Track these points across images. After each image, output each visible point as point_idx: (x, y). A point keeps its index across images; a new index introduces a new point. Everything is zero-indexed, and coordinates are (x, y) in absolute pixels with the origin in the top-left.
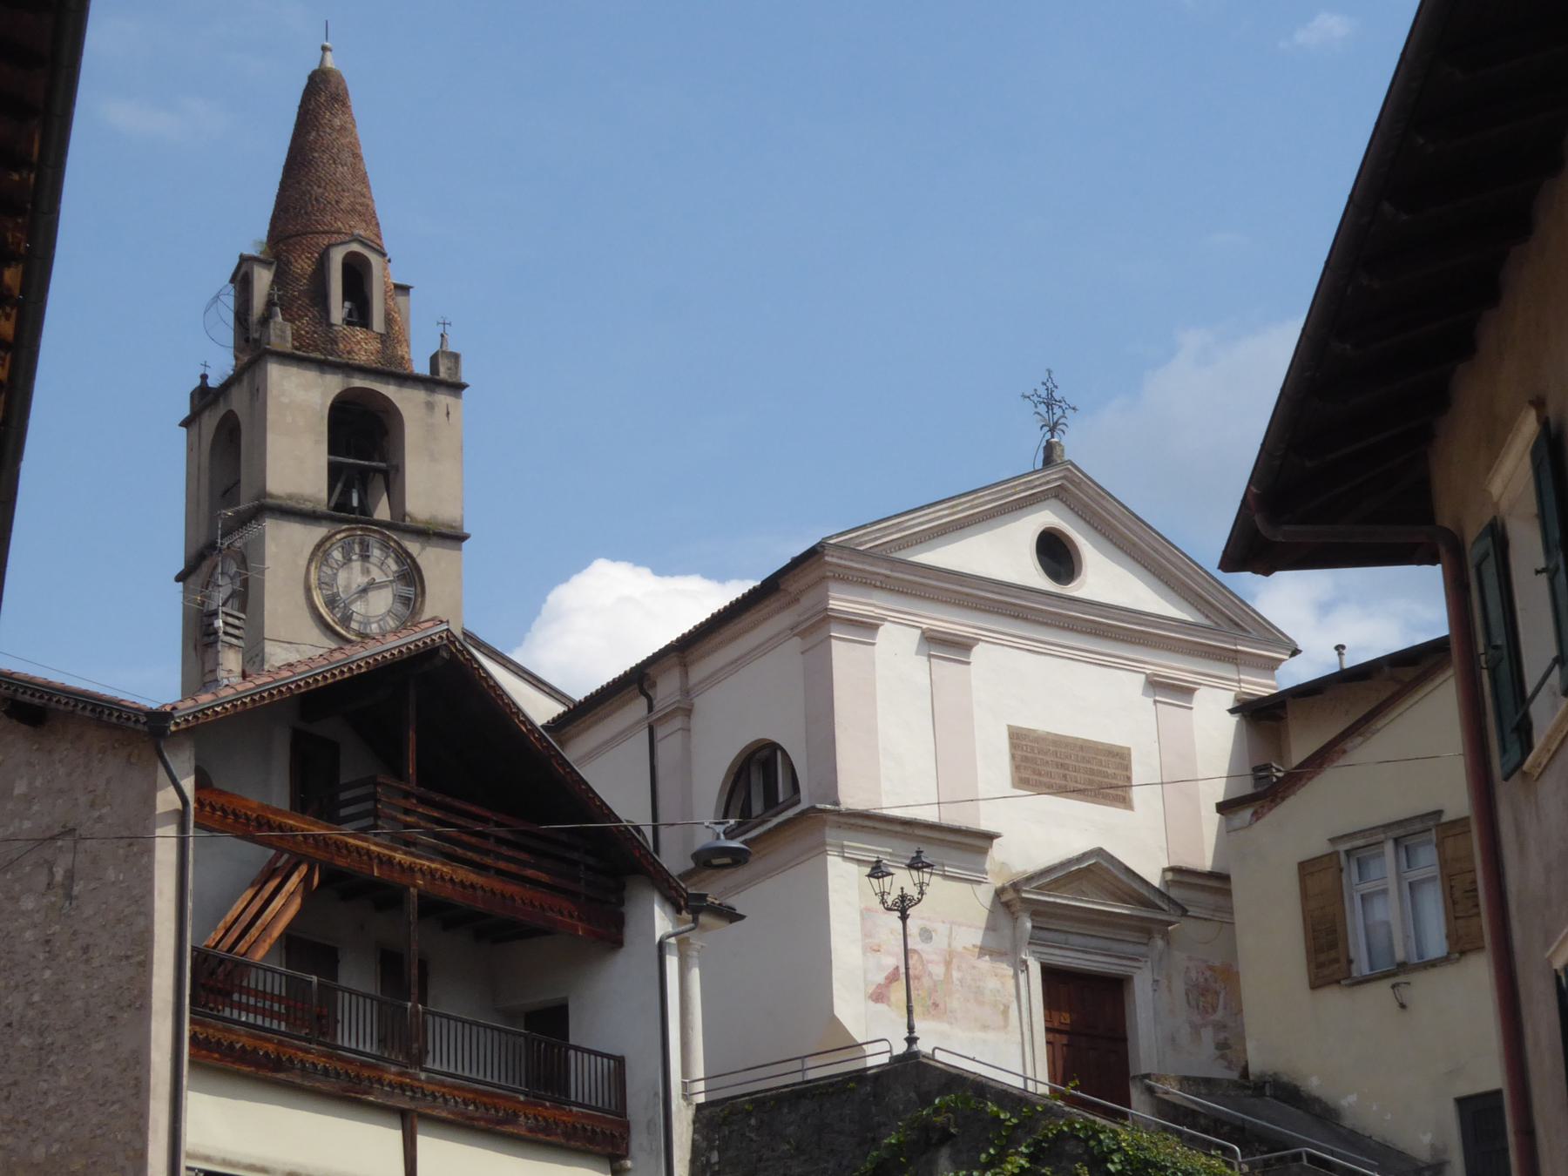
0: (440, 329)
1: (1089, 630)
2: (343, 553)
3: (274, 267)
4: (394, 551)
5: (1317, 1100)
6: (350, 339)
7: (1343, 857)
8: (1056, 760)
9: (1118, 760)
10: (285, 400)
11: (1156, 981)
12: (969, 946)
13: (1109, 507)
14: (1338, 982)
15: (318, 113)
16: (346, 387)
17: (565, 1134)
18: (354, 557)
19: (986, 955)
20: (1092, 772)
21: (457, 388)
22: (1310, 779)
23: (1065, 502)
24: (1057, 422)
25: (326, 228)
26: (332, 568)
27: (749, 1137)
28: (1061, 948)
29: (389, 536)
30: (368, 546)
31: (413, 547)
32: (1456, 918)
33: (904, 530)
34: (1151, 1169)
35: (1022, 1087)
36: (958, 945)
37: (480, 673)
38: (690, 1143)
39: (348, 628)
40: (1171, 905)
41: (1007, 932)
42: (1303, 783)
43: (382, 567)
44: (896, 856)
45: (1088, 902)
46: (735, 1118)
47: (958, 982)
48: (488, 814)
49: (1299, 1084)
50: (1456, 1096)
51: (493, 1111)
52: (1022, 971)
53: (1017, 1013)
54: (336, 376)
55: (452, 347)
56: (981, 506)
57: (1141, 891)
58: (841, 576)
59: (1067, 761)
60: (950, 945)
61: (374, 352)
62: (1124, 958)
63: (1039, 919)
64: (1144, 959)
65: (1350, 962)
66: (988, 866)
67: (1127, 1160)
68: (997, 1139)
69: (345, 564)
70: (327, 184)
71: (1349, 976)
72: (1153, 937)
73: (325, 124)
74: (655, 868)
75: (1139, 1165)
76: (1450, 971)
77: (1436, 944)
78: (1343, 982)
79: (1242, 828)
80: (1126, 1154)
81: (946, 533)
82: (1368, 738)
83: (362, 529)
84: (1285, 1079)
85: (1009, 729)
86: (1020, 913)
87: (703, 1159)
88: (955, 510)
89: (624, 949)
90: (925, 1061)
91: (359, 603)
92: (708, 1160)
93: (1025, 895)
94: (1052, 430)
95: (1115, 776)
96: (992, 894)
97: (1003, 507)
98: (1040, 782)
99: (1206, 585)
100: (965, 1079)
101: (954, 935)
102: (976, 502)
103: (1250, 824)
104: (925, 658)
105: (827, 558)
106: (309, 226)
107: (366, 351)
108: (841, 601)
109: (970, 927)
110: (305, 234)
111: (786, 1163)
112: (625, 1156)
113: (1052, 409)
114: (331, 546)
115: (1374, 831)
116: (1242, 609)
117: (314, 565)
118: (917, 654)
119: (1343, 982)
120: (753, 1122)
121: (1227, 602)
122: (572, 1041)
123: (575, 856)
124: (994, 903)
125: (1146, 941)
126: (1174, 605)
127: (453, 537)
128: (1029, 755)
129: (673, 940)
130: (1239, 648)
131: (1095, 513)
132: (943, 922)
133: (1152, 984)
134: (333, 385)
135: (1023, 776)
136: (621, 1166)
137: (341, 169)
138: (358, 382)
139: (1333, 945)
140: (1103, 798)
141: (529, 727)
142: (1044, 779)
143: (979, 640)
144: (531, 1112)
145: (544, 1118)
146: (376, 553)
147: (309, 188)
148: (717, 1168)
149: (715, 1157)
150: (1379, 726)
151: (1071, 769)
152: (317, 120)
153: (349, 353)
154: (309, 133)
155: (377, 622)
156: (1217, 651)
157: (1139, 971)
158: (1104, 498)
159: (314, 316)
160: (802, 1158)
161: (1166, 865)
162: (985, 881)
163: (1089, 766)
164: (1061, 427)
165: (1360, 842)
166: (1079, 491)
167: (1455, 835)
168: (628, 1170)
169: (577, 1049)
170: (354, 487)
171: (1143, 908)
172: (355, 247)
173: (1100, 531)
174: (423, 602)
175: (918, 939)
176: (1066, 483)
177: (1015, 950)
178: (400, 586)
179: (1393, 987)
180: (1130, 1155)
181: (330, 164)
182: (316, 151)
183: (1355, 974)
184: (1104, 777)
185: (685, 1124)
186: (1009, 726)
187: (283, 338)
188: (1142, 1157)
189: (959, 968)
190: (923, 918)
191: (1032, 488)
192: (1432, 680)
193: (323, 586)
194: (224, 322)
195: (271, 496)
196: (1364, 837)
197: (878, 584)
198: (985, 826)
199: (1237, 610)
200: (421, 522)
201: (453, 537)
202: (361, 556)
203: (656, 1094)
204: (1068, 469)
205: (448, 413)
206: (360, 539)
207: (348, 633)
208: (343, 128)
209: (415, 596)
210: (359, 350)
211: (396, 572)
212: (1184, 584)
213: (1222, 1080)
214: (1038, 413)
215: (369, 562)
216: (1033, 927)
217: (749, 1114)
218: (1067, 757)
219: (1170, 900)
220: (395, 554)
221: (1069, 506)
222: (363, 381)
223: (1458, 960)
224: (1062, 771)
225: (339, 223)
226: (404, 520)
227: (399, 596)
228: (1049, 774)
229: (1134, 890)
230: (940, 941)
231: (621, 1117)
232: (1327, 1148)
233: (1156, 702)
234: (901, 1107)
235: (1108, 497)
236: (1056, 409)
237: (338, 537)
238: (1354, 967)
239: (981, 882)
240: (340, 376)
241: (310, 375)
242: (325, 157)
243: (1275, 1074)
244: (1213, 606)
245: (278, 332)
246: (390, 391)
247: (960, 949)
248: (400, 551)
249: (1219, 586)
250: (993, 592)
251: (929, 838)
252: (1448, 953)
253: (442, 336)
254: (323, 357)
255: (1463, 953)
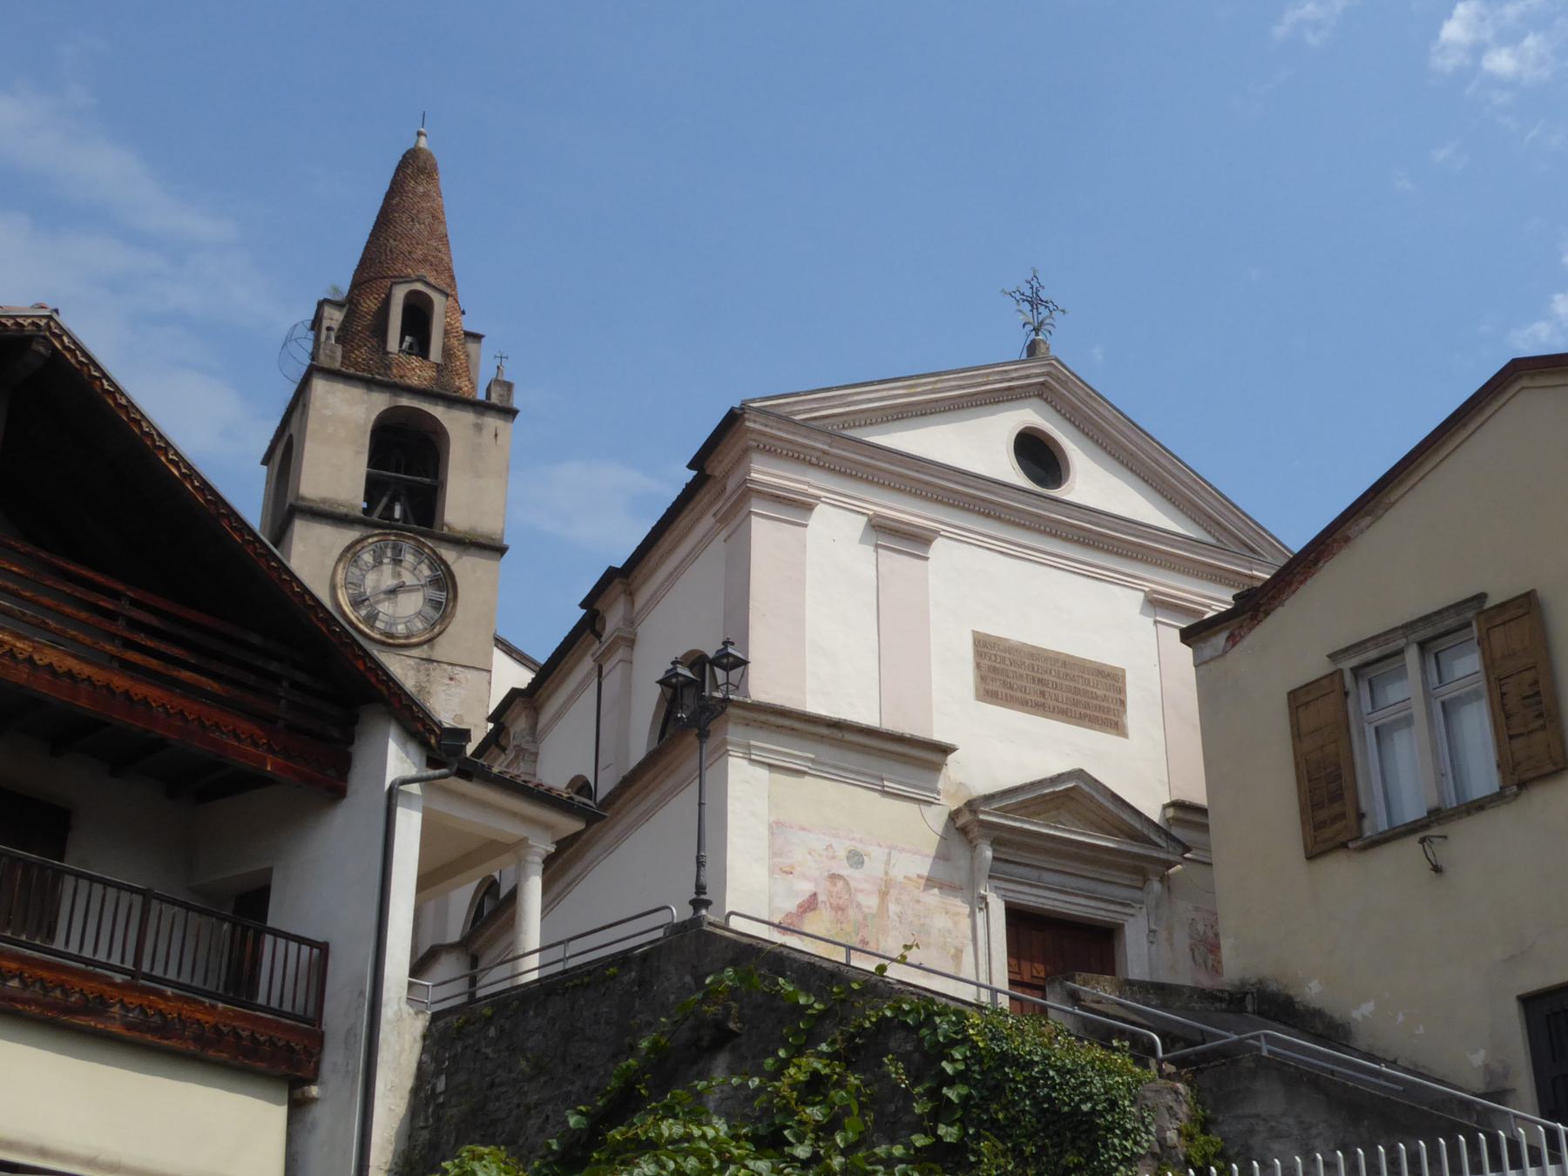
0: (498, 362)
1: (1076, 538)
2: (374, 557)
3: (345, 310)
4: (428, 557)
5: (1318, 1014)
6: (405, 366)
7: (1348, 678)
8: (1032, 674)
9: (1109, 682)
10: (328, 413)
11: (1152, 931)
12: (913, 875)
13: (1101, 409)
14: (1344, 846)
15: (404, 182)
16: (392, 406)
17: (199, 1039)
18: (386, 561)
19: (935, 887)
20: (1077, 691)
21: (509, 413)
22: (1302, 582)
23: (1049, 403)
24: (1042, 322)
25: (395, 273)
26: (361, 569)
27: (485, 1053)
28: (1031, 885)
29: (423, 543)
30: (401, 551)
31: (449, 555)
32: (1511, 737)
33: (848, 404)
34: (1010, 1068)
35: (844, 961)
36: (898, 873)
37: (102, 384)
38: (414, 1065)
39: (372, 627)
40: (1169, 842)
41: (964, 863)
42: (1293, 588)
43: (414, 570)
44: (823, 764)
45: (1064, 830)
46: (471, 1028)
47: (896, 918)
48: (120, 587)
49: (1292, 993)
50: (1520, 993)
51: (58, 993)
52: (981, 909)
53: (972, 958)
54: (383, 395)
55: (506, 378)
56: (947, 391)
57: (1132, 822)
58: (767, 447)
59: (1046, 677)
60: (886, 873)
61: (428, 378)
62: (1113, 902)
63: (1003, 849)
64: (1138, 906)
65: (1361, 816)
66: (940, 785)
67: (977, 1056)
68: (793, 1035)
69: (374, 566)
70: (403, 238)
71: (1359, 836)
72: (1149, 880)
73: (409, 191)
74: (389, 688)
75: (992, 1063)
76: (1501, 817)
77: (1483, 777)
78: (1351, 845)
79: (1213, 659)
80: (974, 1046)
81: (903, 418)
82: (1380, 517)
83: (396, 535)
84: (1274, 987)
85: (974, 635)
86: (980, 841)
87: (428, 1087)
88: (913, 390)
89: (345, 801)
90: (710, 929)
91: (387, 604)
92: (433, 1089)
93: (982, 817)
94: (1037, 330)
95: (1105, 698)
96: (945, 817)
97: (976, 397)
98: (1012, 697)
99: (1216, 503)
100: (760, 950)
101: (893, 861)
102: (939, 385)
103: (1225, 652)
104: (872, 548)
105: (747, 424)
106: (379, 272)
107: (419, 377)
108: (764, 472)
109: (915, 854)
110: (375, 279)
111: (521, 1088)
112: (313, 1080)
113: (1037, 309)
114: (363, 548)
115: (1389, 636)
116: (1259, 534)
117: (341, 565)
118: (862, 541)
119: (1351, 845)
120: (492, 1032)
121: (1240, 524)
122: (270, 923)
123: (274, 667)
124: (947, 826)
125: (1140, 885)
126: (1173, 520)
127: (494, 549)
128: (998, 665)
129: (415, 788)
130: (1255, 573)
131: (1087, 418)
132: (879, 845)
133: (1148, 935)
134: (380, 402)
135: (990, 688)
136: (303, 1093)
137: (418, 226)
138: (405, 401)
139: (1337, 796)
140: (1090, 721)
141: (184, 470)
142: (1018, 694)
143: (937, 533)
144: (133, 999)
145: (160, 1012)
146: (409, 558)
147: (385, 241)
148: (441, 1100)
149: (441, 1085)
150: (1393, 499)
151: (1050, 686)
152: (403, 189)
153: (401, 377)
154: (394, 198)
155: (405, 623)
156: (1231, 576)
157: (1131, 920)
158: (1095, 400)
159: (373, 345)
160: (542, 1079)
161: (1167, 801)
162: (936, 802)
163: (1073, 684)
164: (1046, 327)
165: (1373, 654)
166: (1066, 390)
167: (1504, 623)
168: (314, 1100)
169: (277, 933)
170: (399, 500)
171: (1134, 843)
172: (419, 286)
173: (1092, 437)
174: (454, 606)
175: (845, 862)
176: (1050, 380)
177: (972, 884)
178: (431, 591)
179: (1422, 841)
180: (981, 1049)
181: (408, 222)
182: (397, 212)
183: (1368, 833)
184: (1092, 698)
185: (408, 1038)
186: (974, 632)
187: (332, 358)
188: (998, 1050)
189: (898, 901)
190: (853, 839)
191: (1010, 381)
192: (1465, 425)
193: (349, 586)
194: (294, 358)
195: (303, 499)
196: (1377, 646)
197: (814, 460)
198: (938, 736)
199: (1252, 534)
200: (459, 532)
201: (494, 549)
202: (394, 560)
203: (362, 993)
204: (1051, 365)
205: (496, 435)
206: (394, 544)
207: (372, 631)
208: (426, 194)
209: (447, 599)
210: (413, 375)
211: (428, 577)
212: (1190, 501)
213: (1183, 986)
214: (1021, 311)
215: (400, 566)
216: (995, 858)
217: (489, 1020)
218: (1046, 672)
219: (1169, 836)
220: (429, 560)
221: (1055, 407)
222: (412, 401)
223: (1517, 795)
224: (1039, 687)
225: (409, 270)
226: (442, 529)
227: (430, 600)
228: (1024, 690)
229: (1125, 823)
230: (874, 866)
231: (314, 1026)
232: (1327, 1068)
233: (1156, 622)
234: (672, 998)
235: (1099, 399)
236: (1041, 309)
237: (370, 540)
238: (1367, 823)
239: (932, 803)
240: (388, 394)
241: (357, 392)
242: (404, 216)
243: (1261, 982)
244: (1225, 529)
245: (328, 352)
246: (438, 411)
247: (900, 878)
248: (435, 557)
249: (1231, 507)
250: (957, 483)
251: (865, 746)
252: (1501, 788)
253: (498, 368)
254: (370, 376)
255: (1523, 785)
